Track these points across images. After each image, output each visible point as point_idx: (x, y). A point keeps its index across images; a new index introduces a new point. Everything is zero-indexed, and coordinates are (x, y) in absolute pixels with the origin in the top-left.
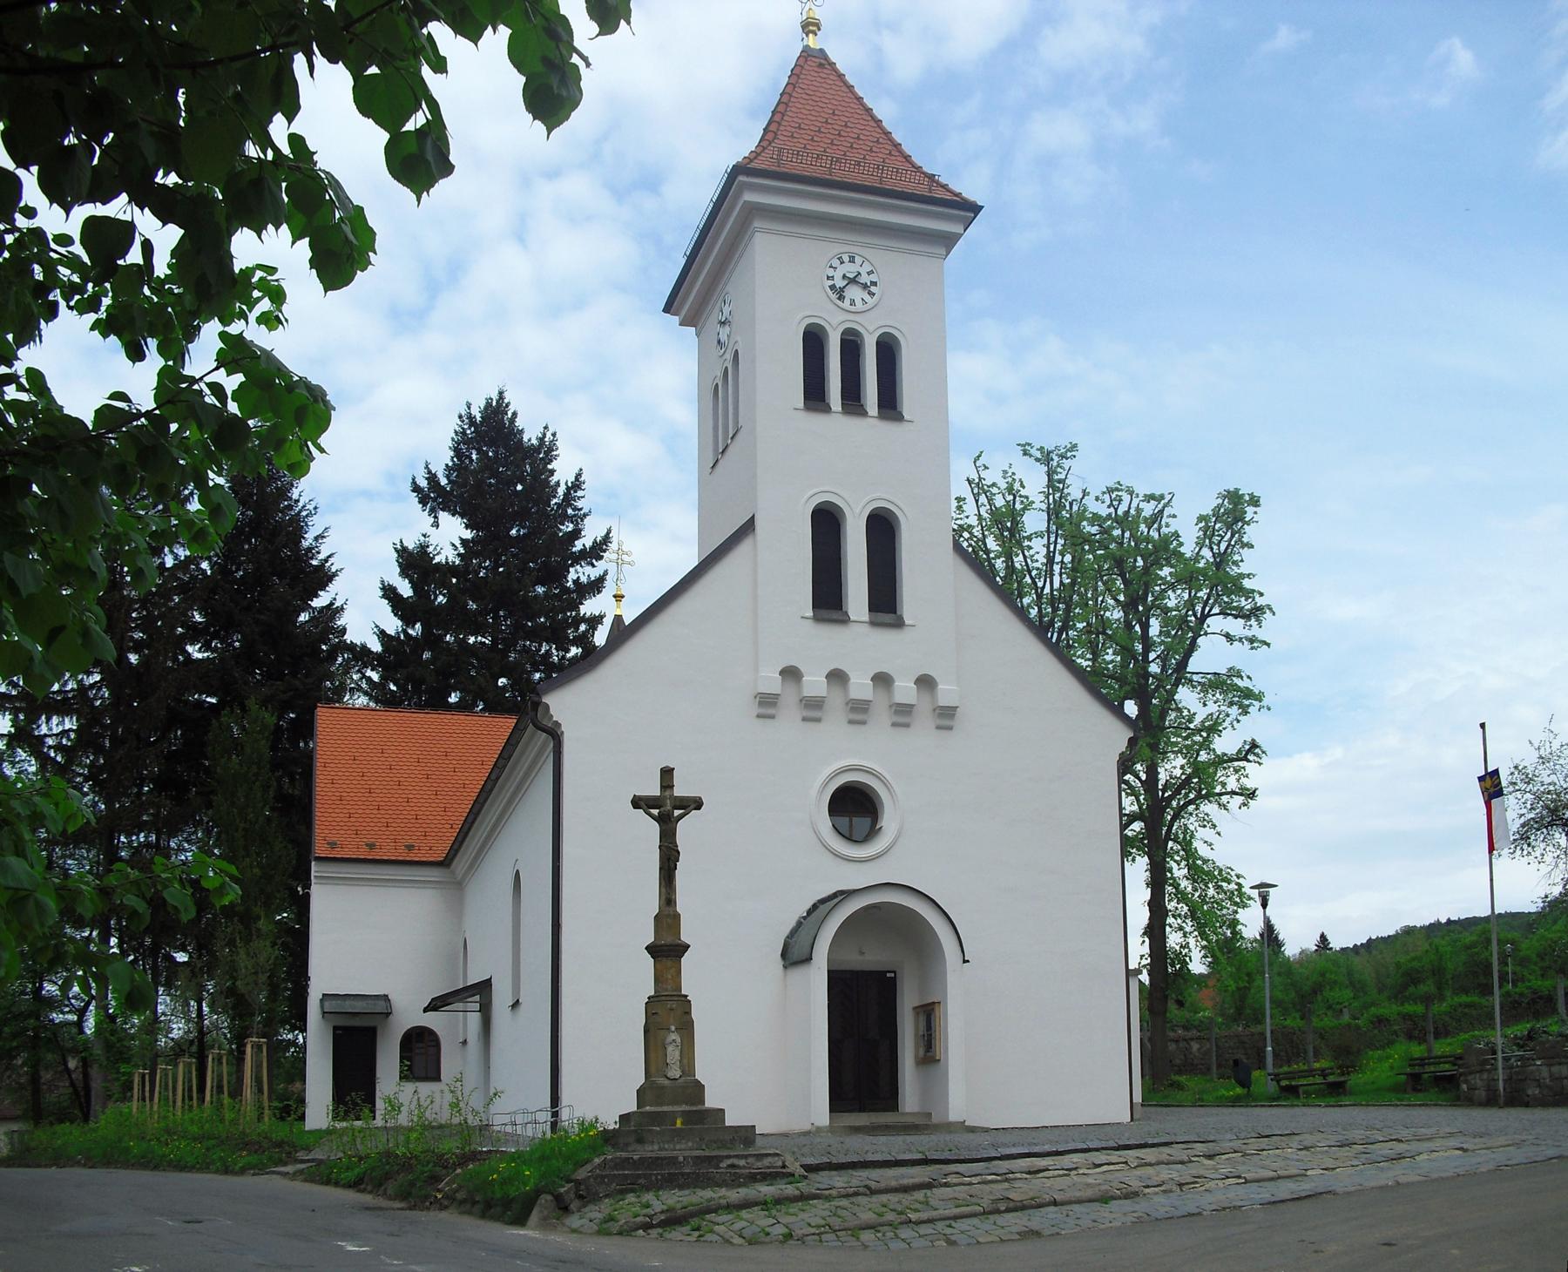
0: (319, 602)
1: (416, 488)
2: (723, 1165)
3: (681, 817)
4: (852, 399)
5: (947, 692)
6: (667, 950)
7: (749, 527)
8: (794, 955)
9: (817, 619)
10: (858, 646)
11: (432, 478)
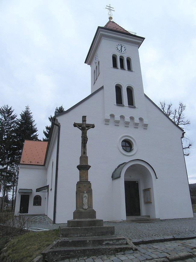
0: (35, 134)
1: (49, 119)
2: (104, 243)
3: (88, 129)
4: (122, 67)
5: (146, 121)
6: (84, 167)
7: (102, 88)
8: (115, 176)
9: (117, 105)
10: (126, 111)
11: (51, 117)
